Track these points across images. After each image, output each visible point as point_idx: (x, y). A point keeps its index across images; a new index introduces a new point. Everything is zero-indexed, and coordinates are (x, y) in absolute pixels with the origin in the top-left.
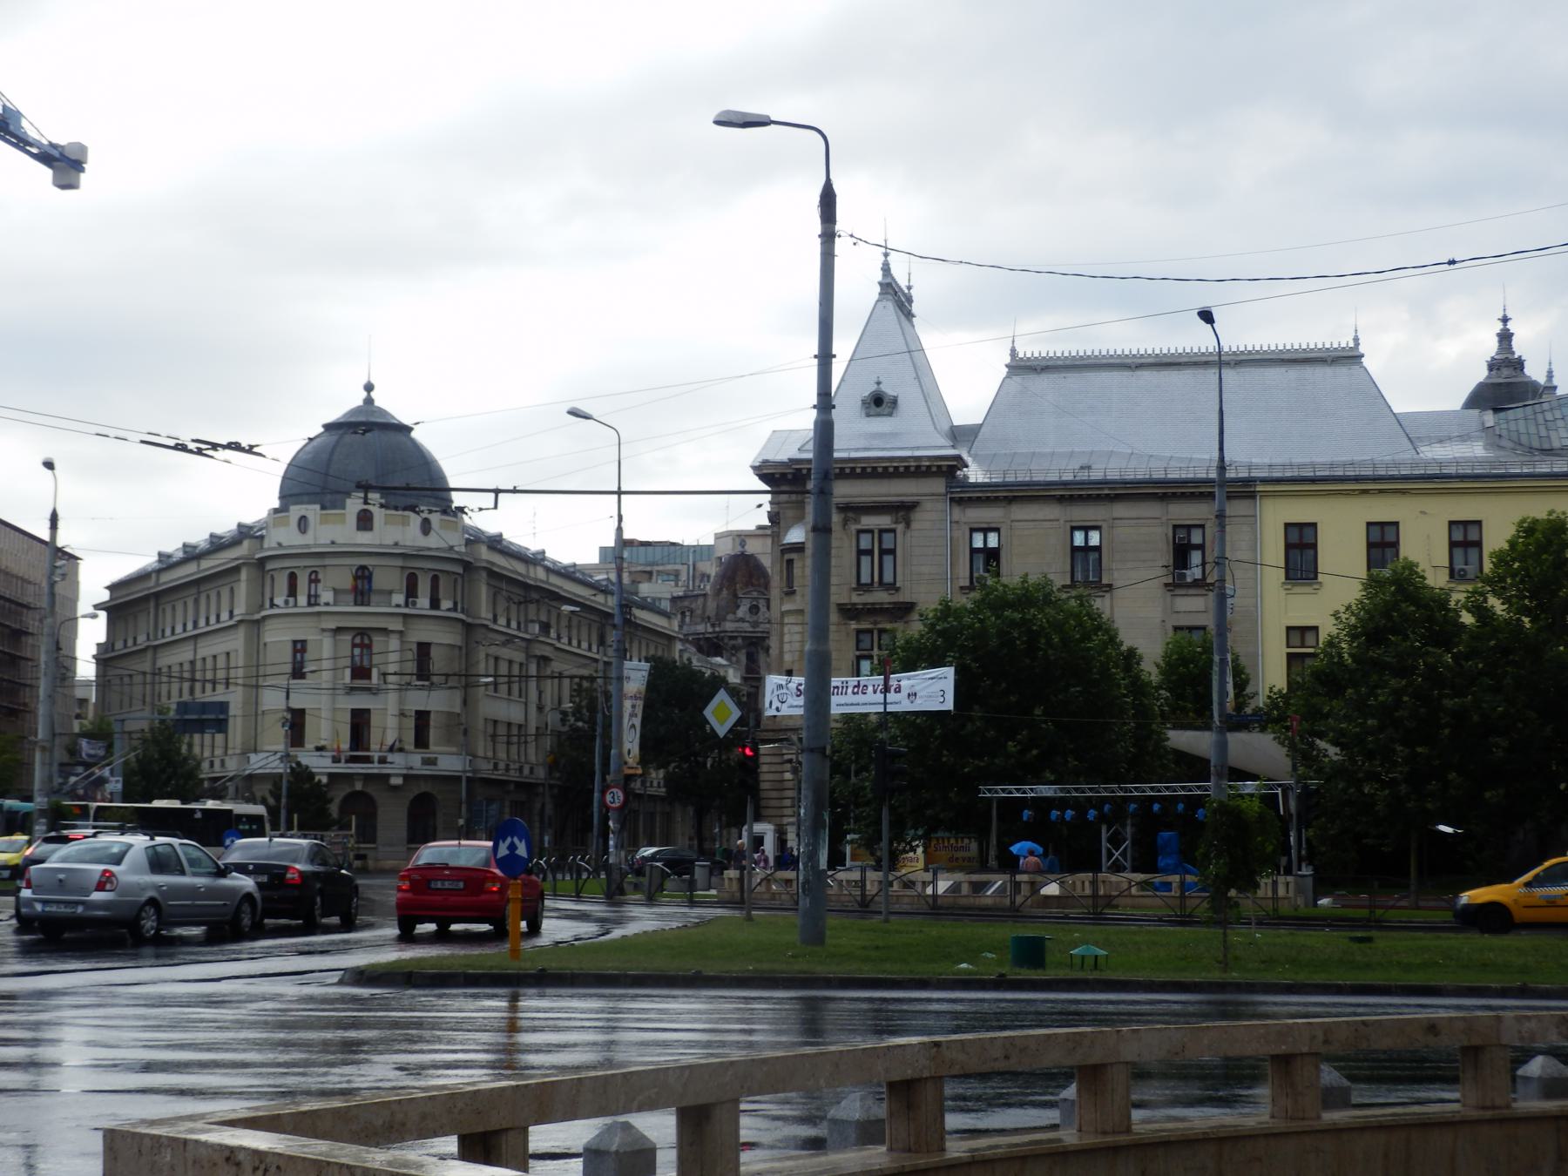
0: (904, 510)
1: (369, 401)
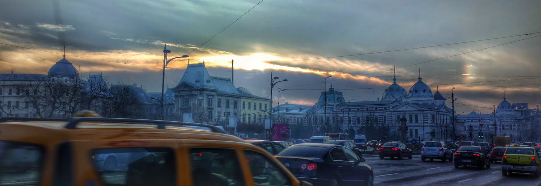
0: (213, 96)
1: (64, 58)
